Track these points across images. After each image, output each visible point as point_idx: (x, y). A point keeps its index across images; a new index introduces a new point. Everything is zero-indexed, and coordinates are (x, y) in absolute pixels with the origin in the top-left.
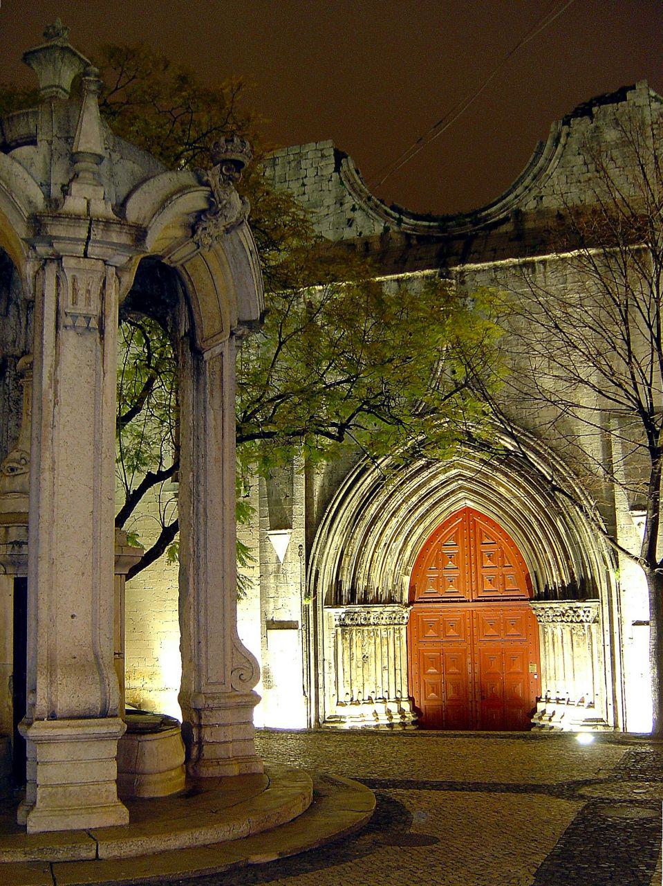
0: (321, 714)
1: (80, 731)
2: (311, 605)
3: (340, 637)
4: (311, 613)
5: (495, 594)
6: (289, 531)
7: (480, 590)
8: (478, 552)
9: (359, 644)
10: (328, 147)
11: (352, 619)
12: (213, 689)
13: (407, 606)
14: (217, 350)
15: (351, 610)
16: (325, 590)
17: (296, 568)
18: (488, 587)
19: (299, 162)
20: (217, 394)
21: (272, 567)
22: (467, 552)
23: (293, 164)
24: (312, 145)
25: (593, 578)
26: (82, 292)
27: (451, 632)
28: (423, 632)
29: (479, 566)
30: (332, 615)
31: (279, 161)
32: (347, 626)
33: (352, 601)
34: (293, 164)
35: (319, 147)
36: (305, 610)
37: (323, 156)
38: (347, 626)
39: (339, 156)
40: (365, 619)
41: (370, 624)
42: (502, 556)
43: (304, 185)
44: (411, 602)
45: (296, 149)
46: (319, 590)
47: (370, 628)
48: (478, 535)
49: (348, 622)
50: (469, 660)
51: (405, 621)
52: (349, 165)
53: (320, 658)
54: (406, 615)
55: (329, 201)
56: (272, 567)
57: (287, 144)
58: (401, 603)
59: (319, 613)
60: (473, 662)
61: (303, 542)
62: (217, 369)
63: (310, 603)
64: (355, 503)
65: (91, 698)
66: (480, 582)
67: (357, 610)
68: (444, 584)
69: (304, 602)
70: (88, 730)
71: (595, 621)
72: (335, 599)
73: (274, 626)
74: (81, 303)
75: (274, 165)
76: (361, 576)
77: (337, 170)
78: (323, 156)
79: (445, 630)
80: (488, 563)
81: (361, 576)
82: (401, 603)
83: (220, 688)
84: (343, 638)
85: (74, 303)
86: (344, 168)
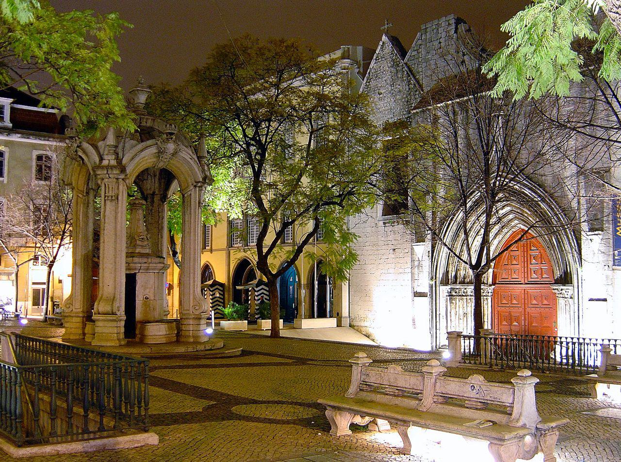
0: (438, 344)
1: (104, 318)
2: (434, 284)
3: (449, 302)
4: (434, 288)
5: (517, 280)
6: (424, 243)
7: (529, 278)
8: (529, 256)
9: (461, 306)
10: (452, 19)
11: (456, 292)
12: (186, 312)
13: (490, 285)
14: (189, 193)
15: (455, 287)
16: (441, 276)
17: (426, 263)
18: (534, 276)
19: (438, 29)
20: (189, 209)
21: (416, 263)
22: (522, 255)
23: (435, 31)
24: (444, 19)
25: (570, 271)
26: (110, 188)
27: (514, 302)
28: (501, 301)
29: (529, 262)
30: (444, 290)
31: (428, 30)
32: (453, 296)
33: (455, 282)
34: (435, 31)
35: (447, 19)
36: (431, 287)
37: (449, 24)
38: (453, 296)
39: (458, 21)
40: (464, 292)
41: (468, 295)
42: (541, 258)
43: (440, 43)
44: (494, 283)
45: (436, 22)
46: (438, 276)
47: (468, 298)
48: (529, 245)
49: (454, 294)
50: (523, 318)
51: (490, 294)
52: (462, 27)
53: (438, 313)
54: (490, 291)
55: (452, 51)
56: (416, 263)
57: (432, 19)
58: (487, 284)
59: (438, 288)
60: (525, 320)
61: (430, 250)
62: (189, 200)
63: (433, 283)
64: (454, 228)
65: (108, 308)
66: (529, 272)
67: (457, 287)
68: (511, 273)
69: (431, 283)
70: (108, 318)
71: (571, 298)
72: (445, 282)
73: (417, 295)
74: (110, 192)
75: (426, 32)
76: (462, 268)
77: (456, 32)
78: (449, 24)
79: (511, 300)
80: (533, 261)
81: (462, 268)
82: (487, 284)
83: (188, 312)
84: (451, 303)
85: (109, 192)
86: (460, 30)
